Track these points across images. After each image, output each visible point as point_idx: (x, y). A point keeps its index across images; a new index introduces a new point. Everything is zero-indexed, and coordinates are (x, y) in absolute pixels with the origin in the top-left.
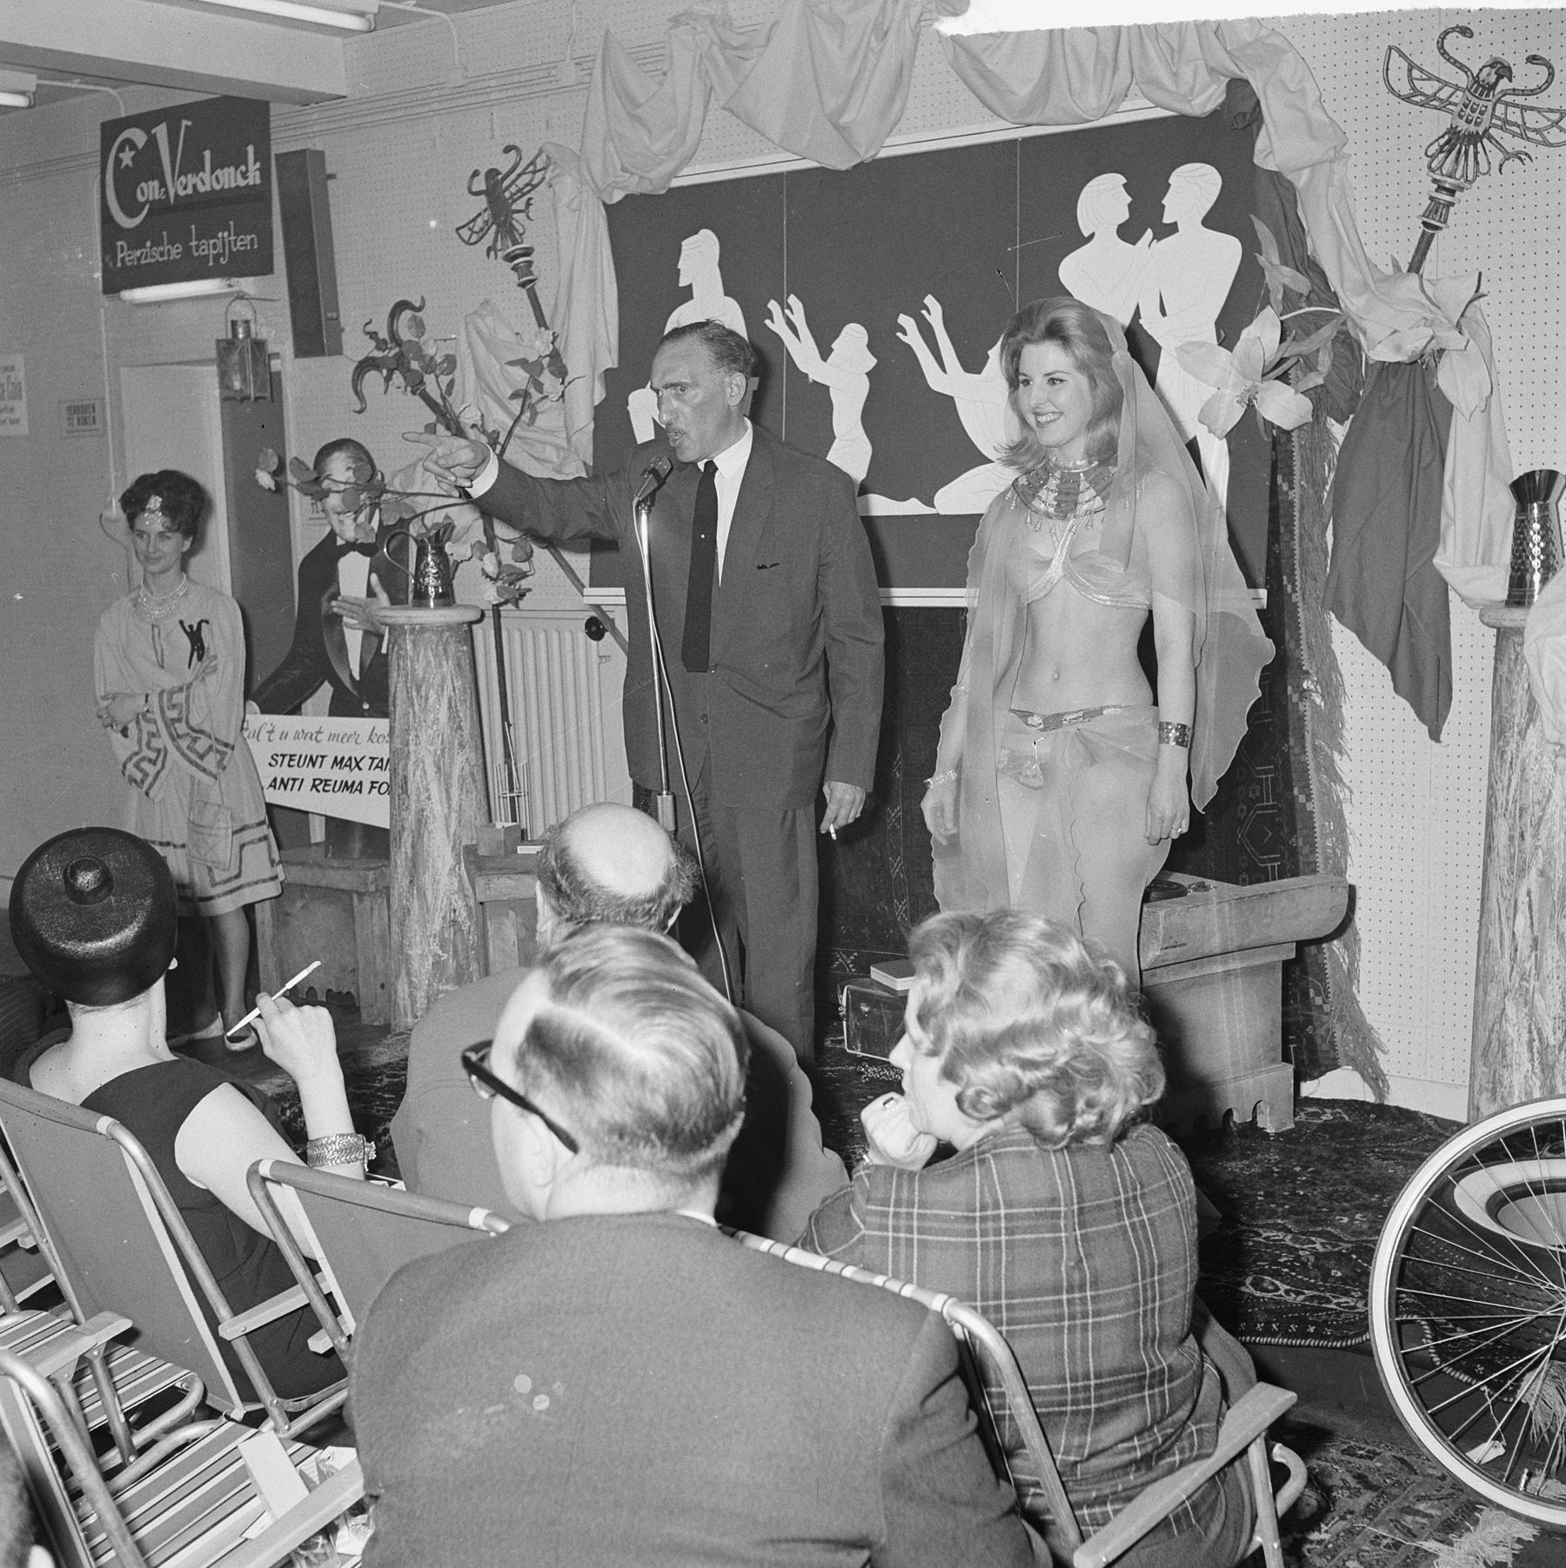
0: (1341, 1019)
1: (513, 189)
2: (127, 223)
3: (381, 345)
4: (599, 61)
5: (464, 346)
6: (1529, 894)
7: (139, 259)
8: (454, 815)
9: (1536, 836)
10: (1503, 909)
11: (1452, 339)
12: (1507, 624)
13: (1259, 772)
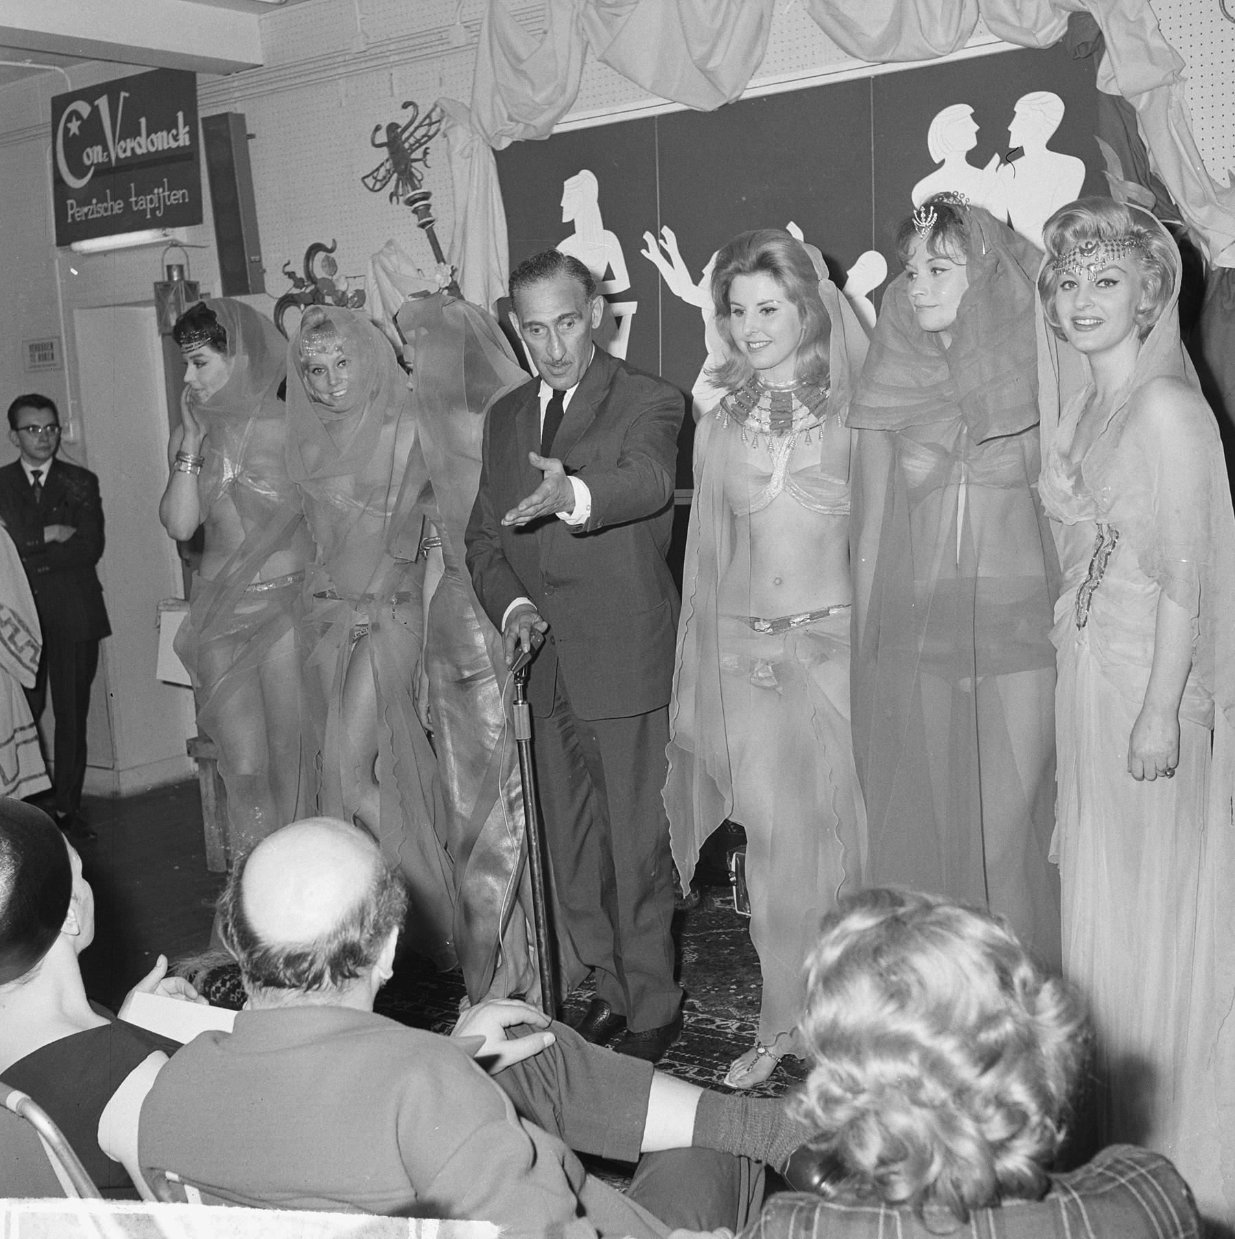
1: (412, 140)
3: (299, 283)
5: (371, 281)
7: (86, 215)
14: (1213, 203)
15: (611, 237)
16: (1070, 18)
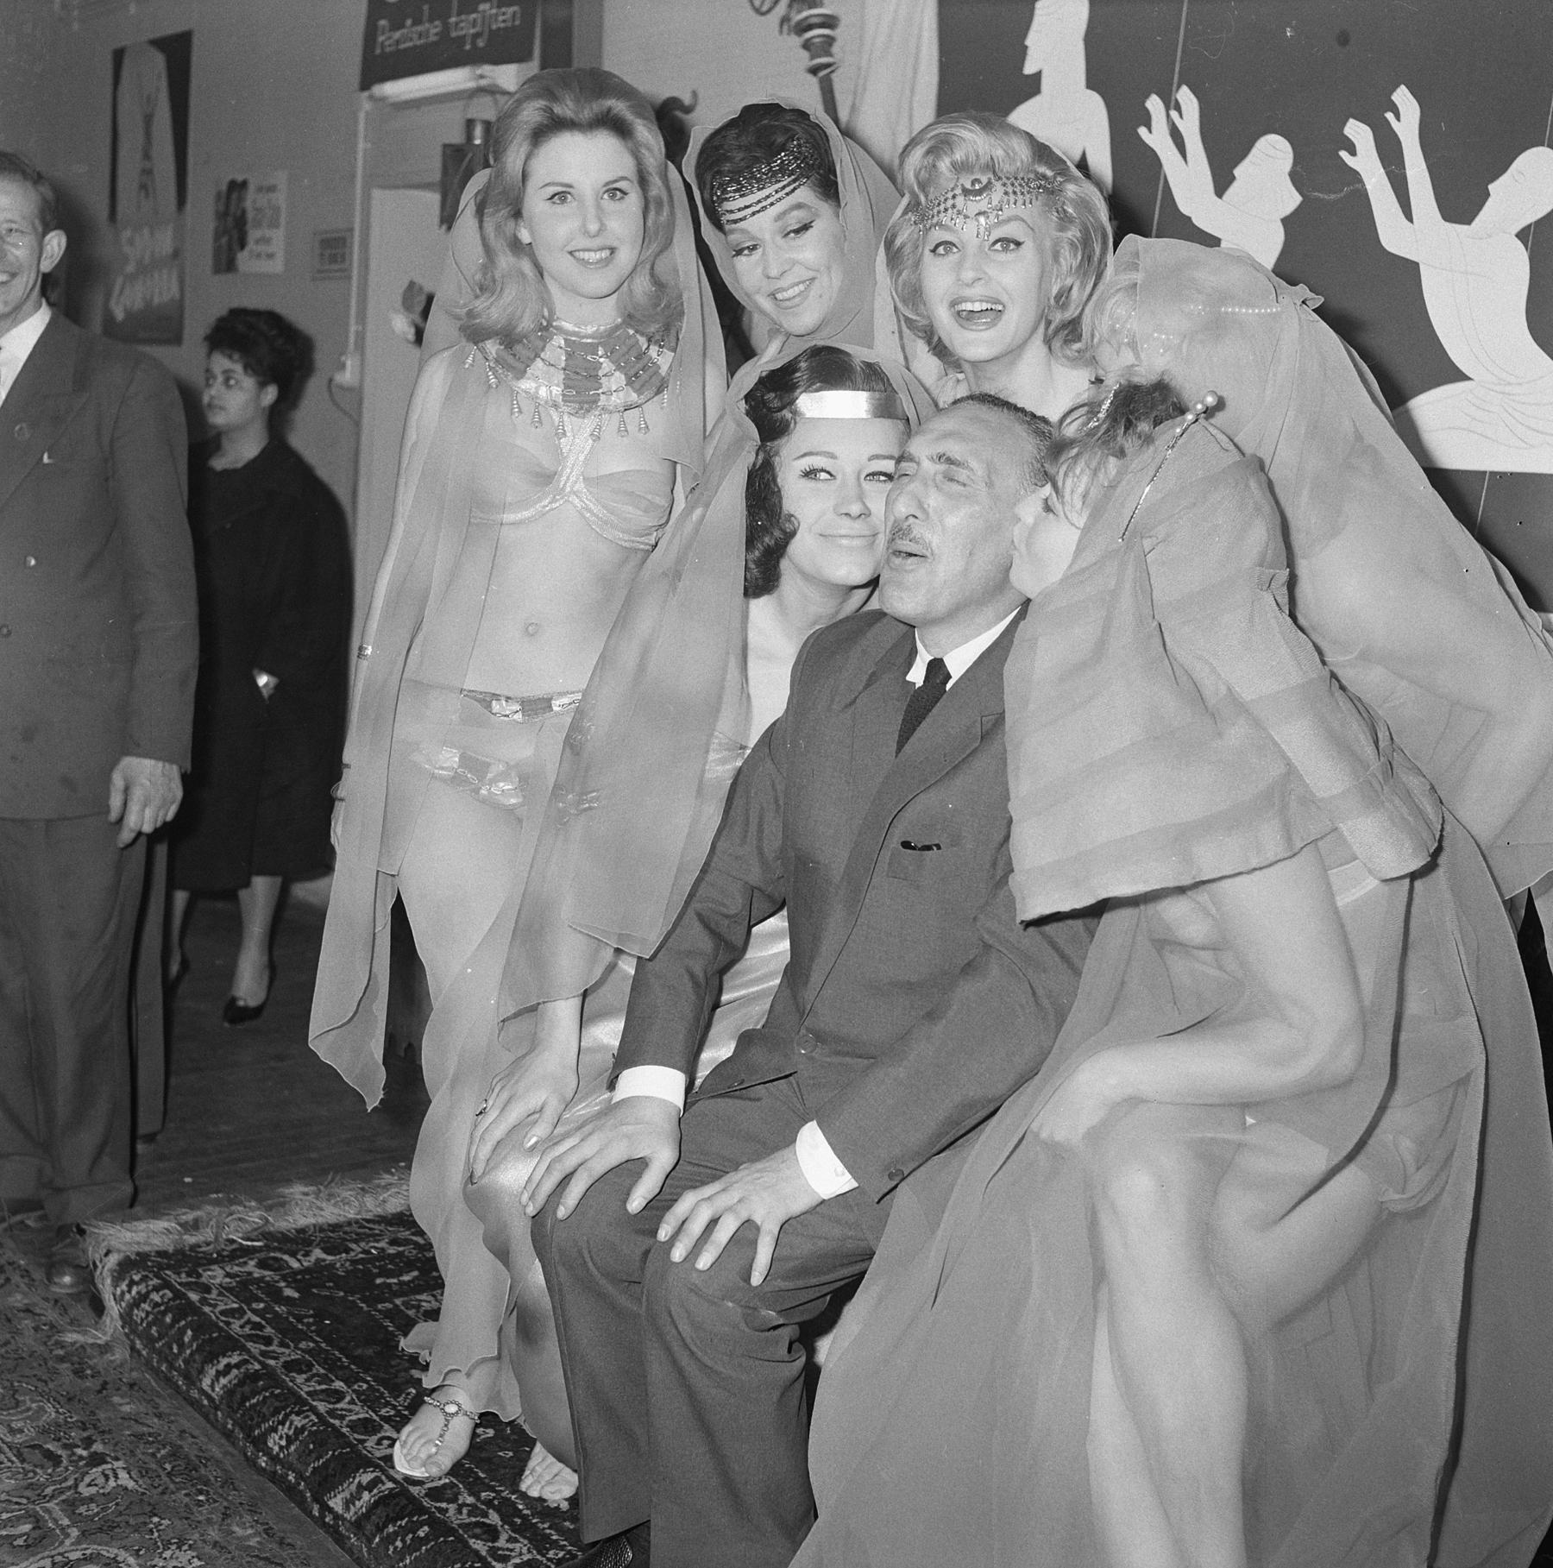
7: (398, 42)
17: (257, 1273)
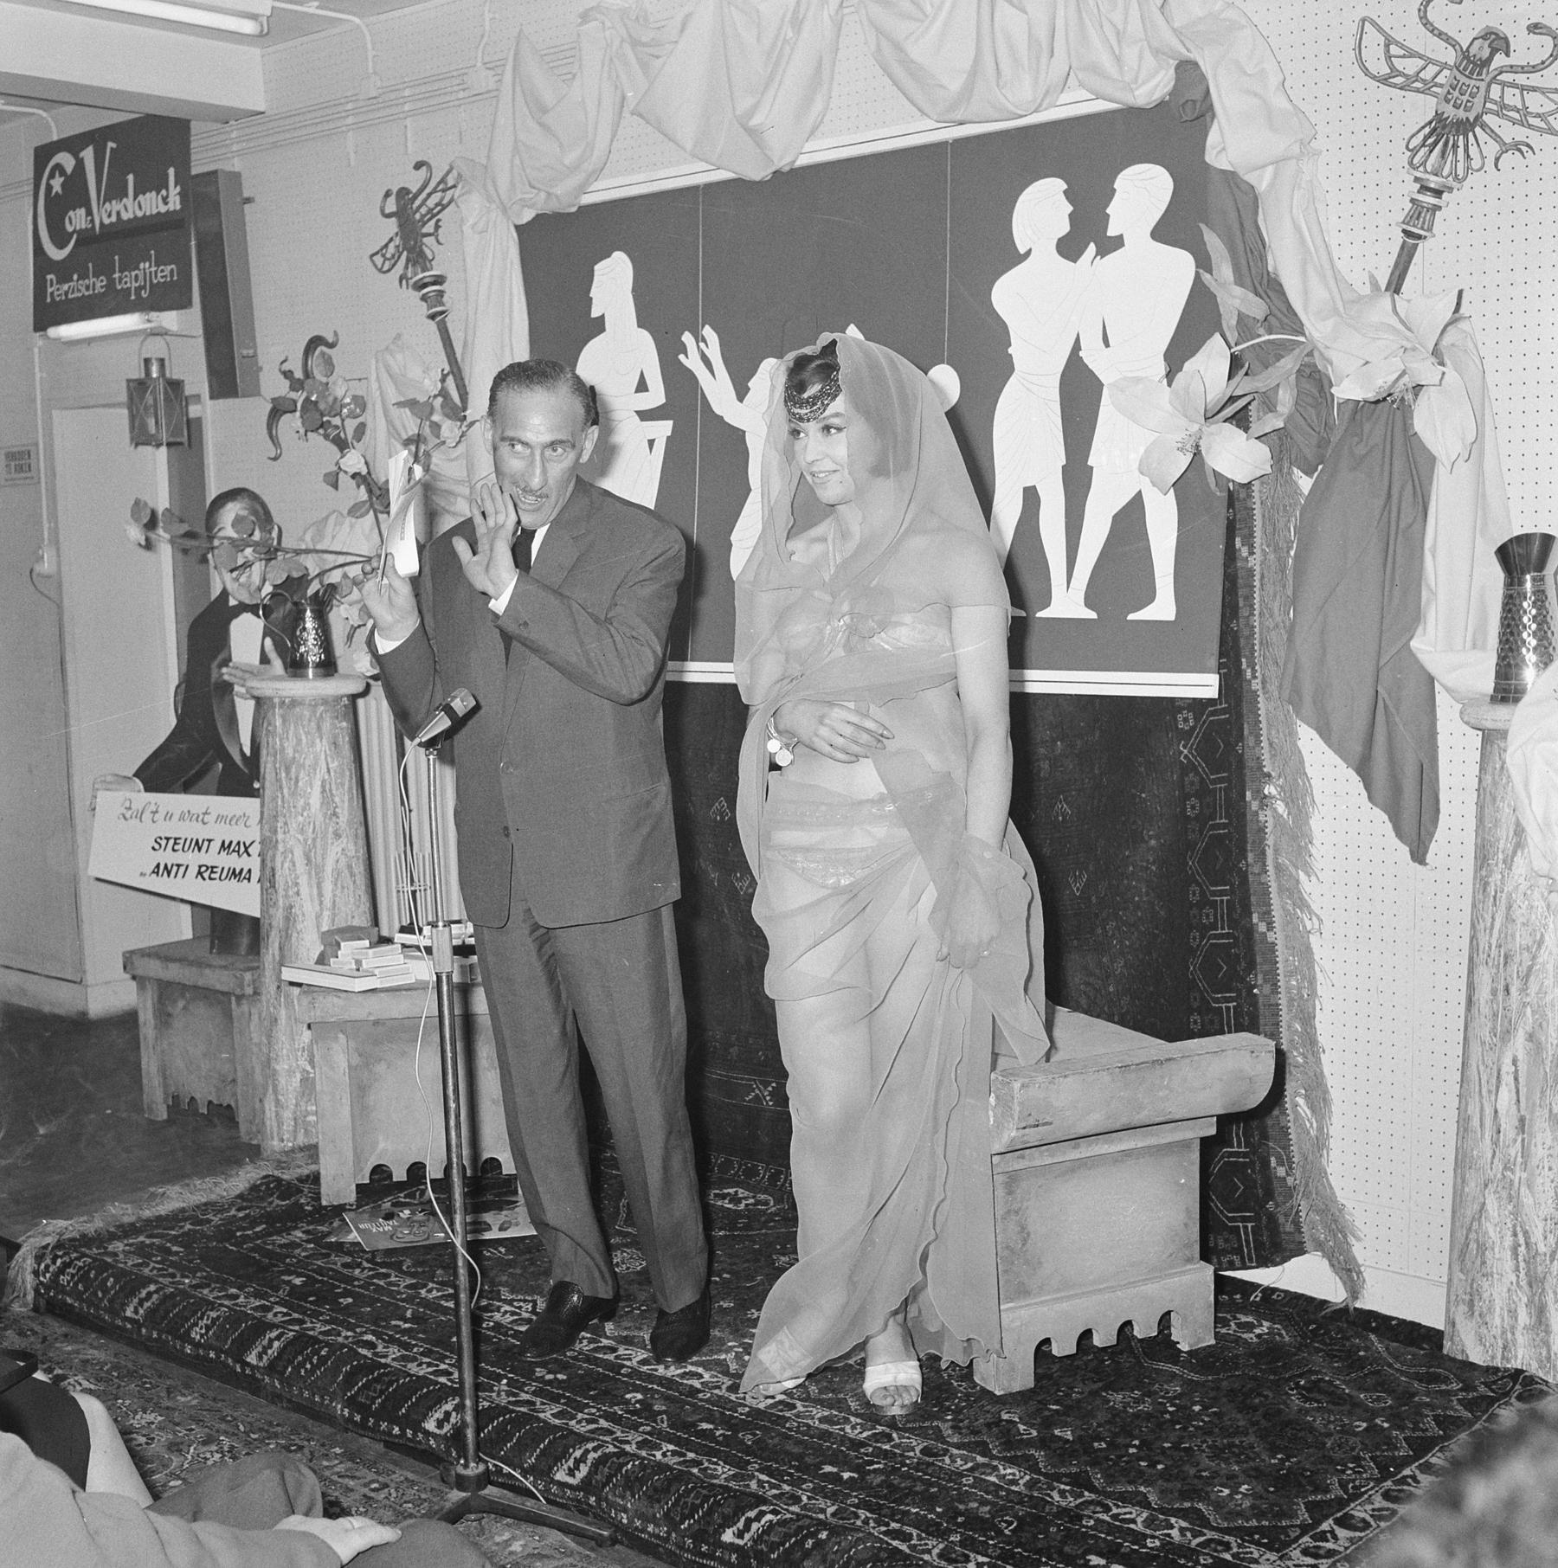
0: (1306, 1195)
1: (423, 210)
2: (56, 254)
3: (296, 385)
4: (509, 68)
5: (375, 386)
6: (1515, 1062)
7: (66, 293)
8: (326, 913)
9: (1524, 990)
10: (1484, 1078)
11: (1426, 371)
12: (1489, 725)
13: (1214, 893)
14: (1340, 316)
15: (646, 338)
16: (1177, 68)
17: (148, 1241)
